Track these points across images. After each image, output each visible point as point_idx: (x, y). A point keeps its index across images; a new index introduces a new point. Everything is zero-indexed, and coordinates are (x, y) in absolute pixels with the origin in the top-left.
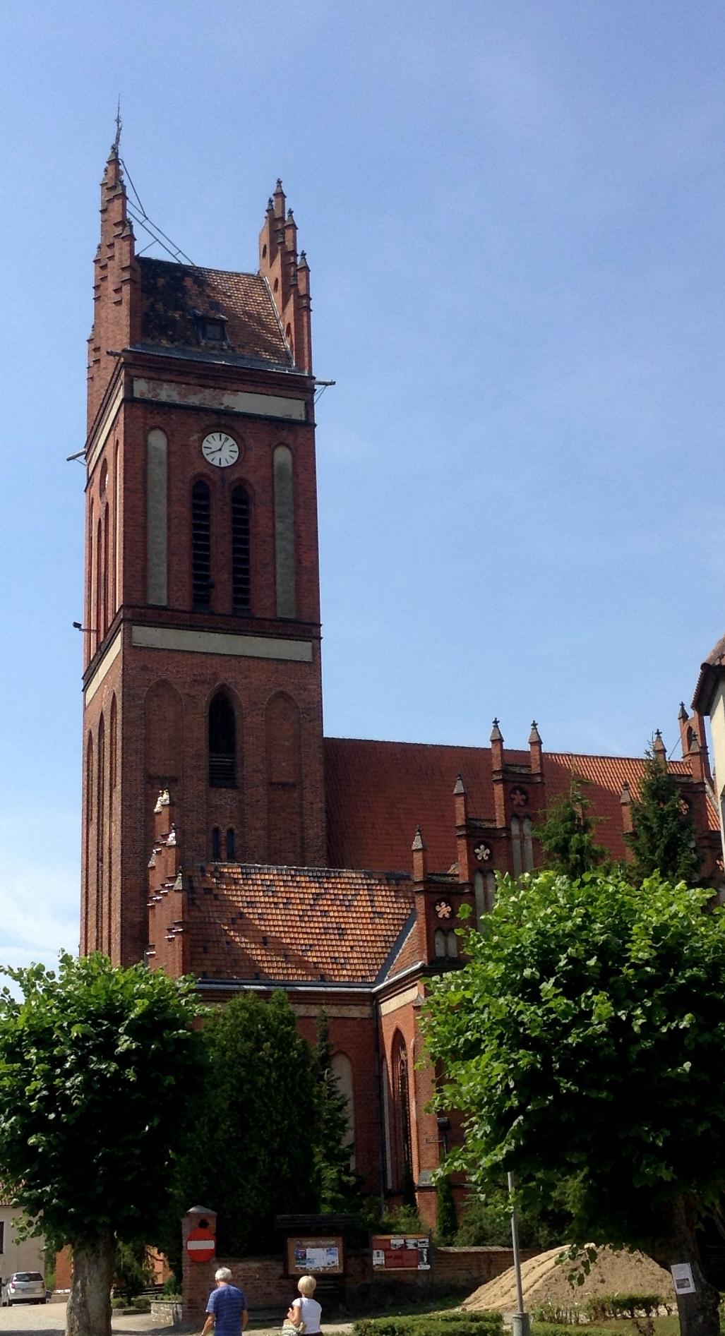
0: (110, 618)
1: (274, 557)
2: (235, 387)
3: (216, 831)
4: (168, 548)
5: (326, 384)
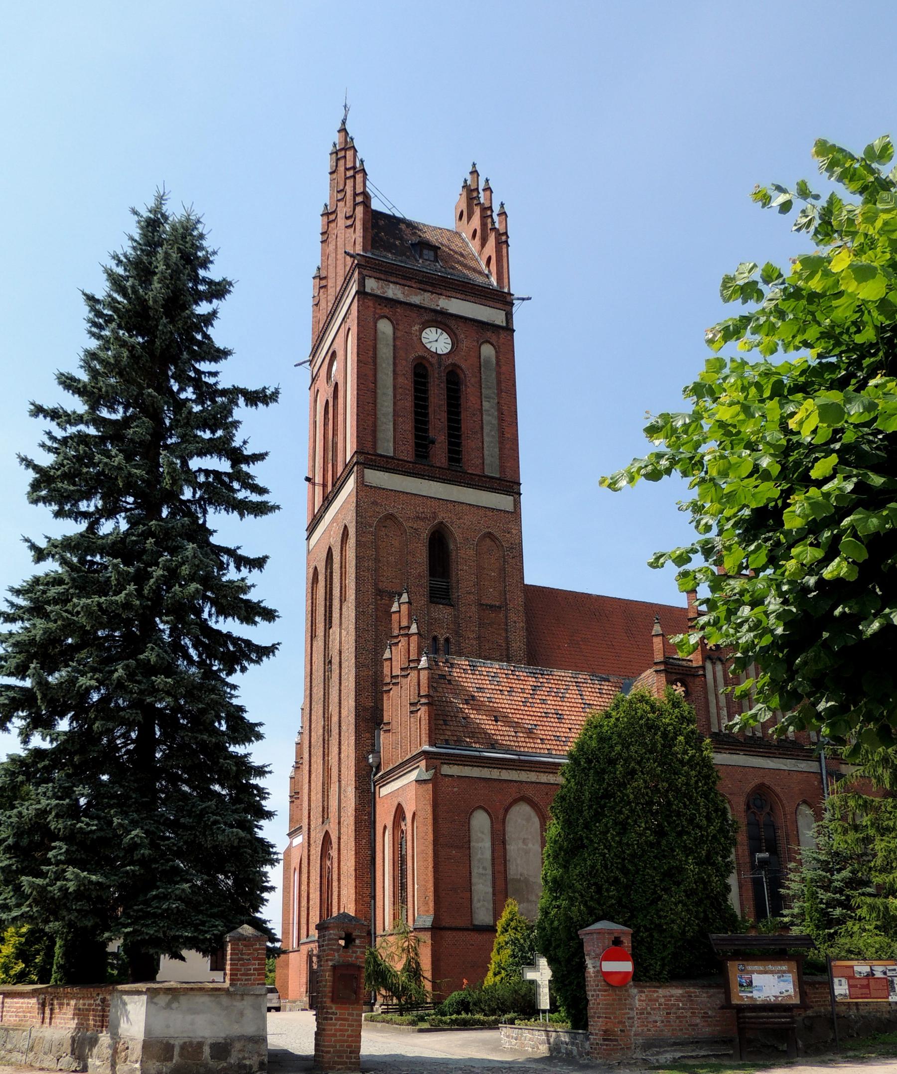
0: (340, 469)
1: (482, 428)
2: (449, 294)
3: (435, 639)
4: (394, 410)
5: (523, 299)
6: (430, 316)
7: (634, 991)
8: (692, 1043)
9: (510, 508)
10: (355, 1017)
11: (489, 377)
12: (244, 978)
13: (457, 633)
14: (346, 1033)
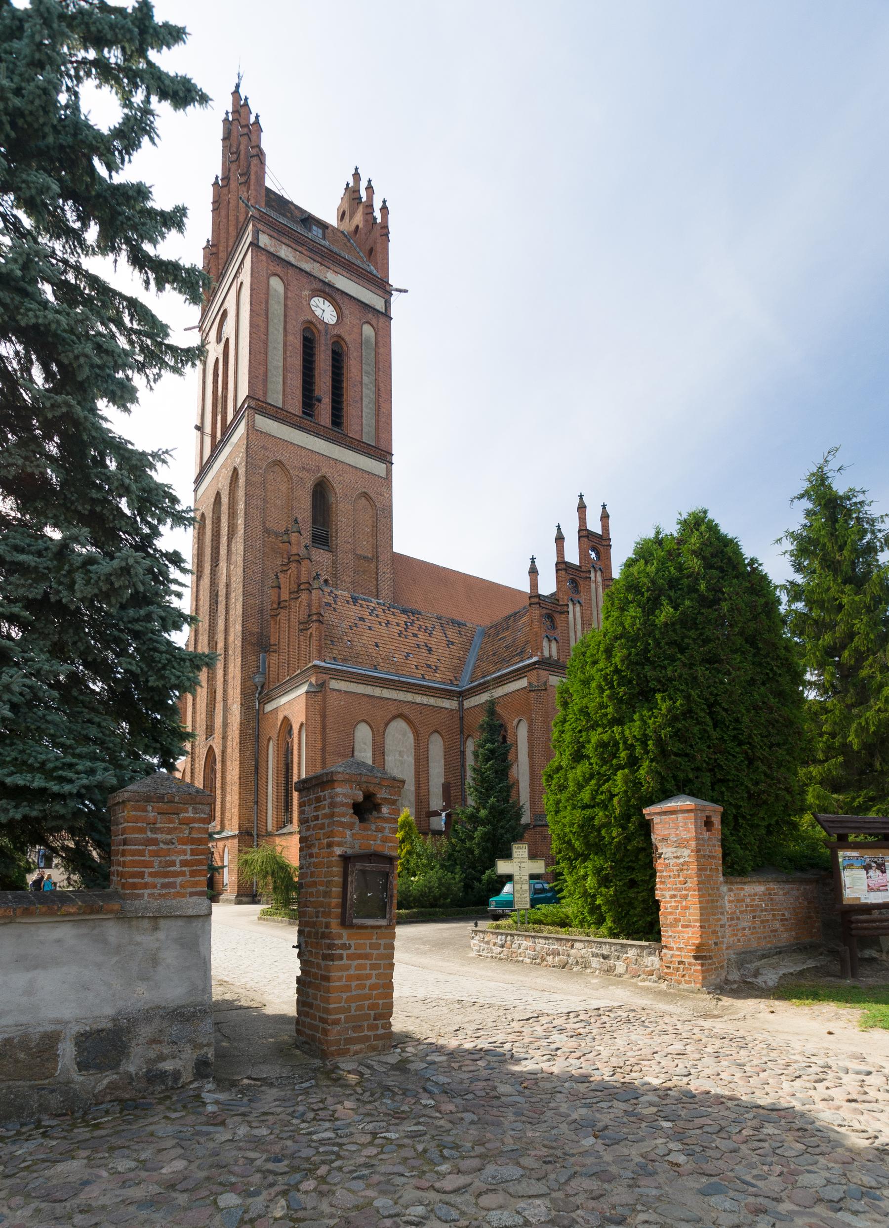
2: (336, 269)
6: (317, 285)
7: (724, 889)
8: (776, 954)
9: (383, 475)
10: (382, 951)
11: (369, 356)
12: (159, 881)
13: (335, 576)
14: (368, 983)
